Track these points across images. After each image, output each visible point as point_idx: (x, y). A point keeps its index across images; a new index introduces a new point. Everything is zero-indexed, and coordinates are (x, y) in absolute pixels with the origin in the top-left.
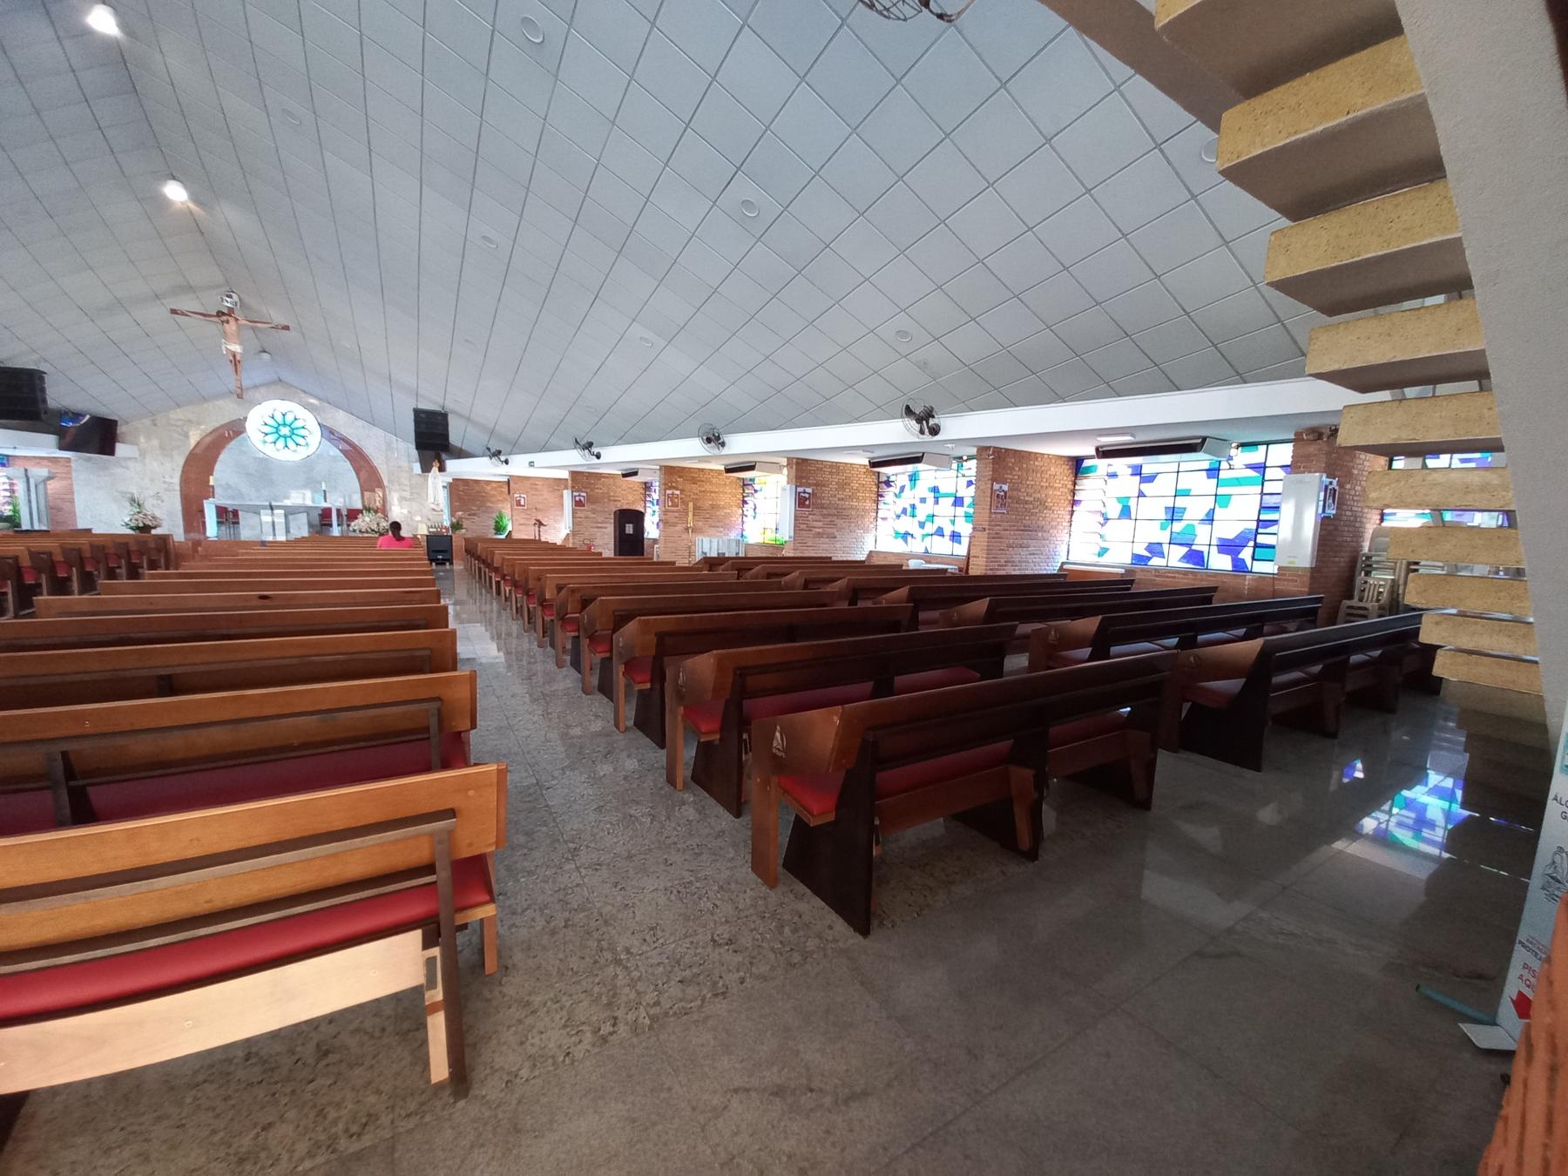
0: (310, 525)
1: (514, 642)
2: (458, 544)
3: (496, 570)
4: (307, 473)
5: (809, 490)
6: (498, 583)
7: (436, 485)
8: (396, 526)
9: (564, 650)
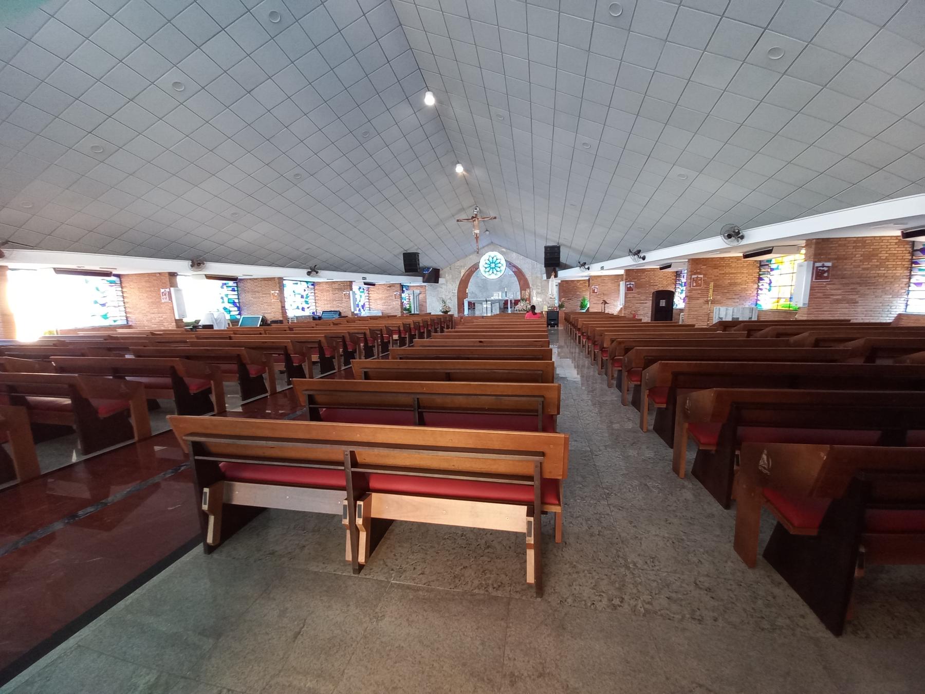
2: (562, 316)
3: (579, 330)
4: (500, 284)
5: (829, 264)
7: (553, 283)
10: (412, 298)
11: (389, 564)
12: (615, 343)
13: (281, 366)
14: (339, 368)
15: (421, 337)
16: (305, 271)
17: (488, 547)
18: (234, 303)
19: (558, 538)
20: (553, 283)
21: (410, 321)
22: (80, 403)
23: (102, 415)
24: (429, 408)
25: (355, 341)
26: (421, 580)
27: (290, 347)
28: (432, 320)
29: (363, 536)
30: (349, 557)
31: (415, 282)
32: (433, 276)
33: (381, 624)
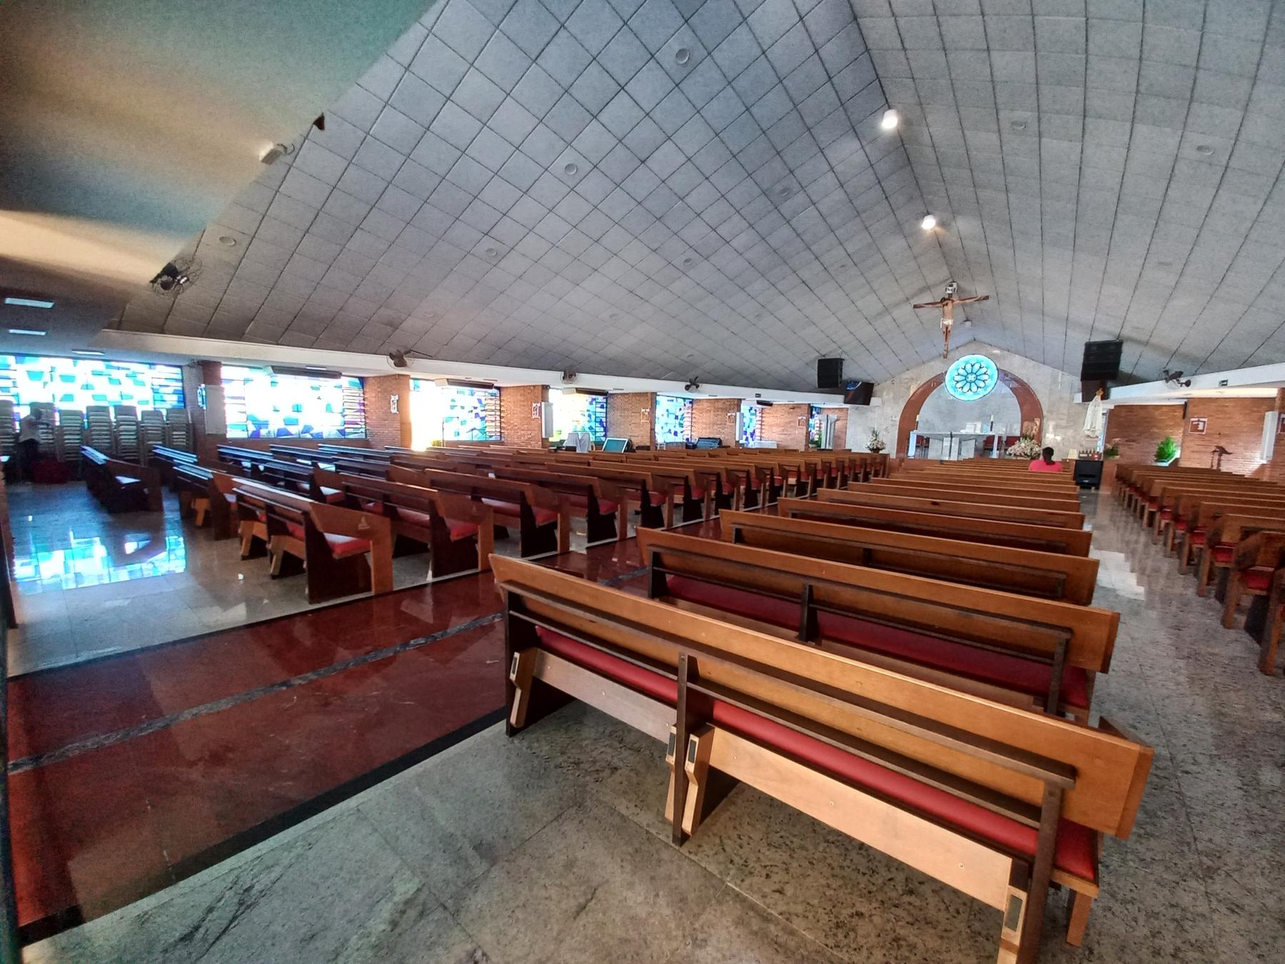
0: (976, 449)
1: (1162, 582)
2: (1110, 468)
3: (1153, 500)
4: (982, 410)
6: (1152, 515)
7: (1096, 414)
8: (1049, 452)
9: (1239, 609)
10: (824, 426)
11: (728, 849)
12: (1253, 540)
13: (635, 505)
14: (708, 516)
15: (831, 484)
16: (684, 384)
17: (911, 892)
18: (601, 422)
19: (1075, 934)
20: (1096, 414)
21: (817, 459)
22: (437, 521)
23: (453, 538)
24: (830, 605)
25: (734, 483)
26: (776, 904)
27: (650, 481)
28: (852, 461)
29: (693, 791)
30: (670, 814)
31: (832, 402)
32: (862, 394)
33: (697, 952)
